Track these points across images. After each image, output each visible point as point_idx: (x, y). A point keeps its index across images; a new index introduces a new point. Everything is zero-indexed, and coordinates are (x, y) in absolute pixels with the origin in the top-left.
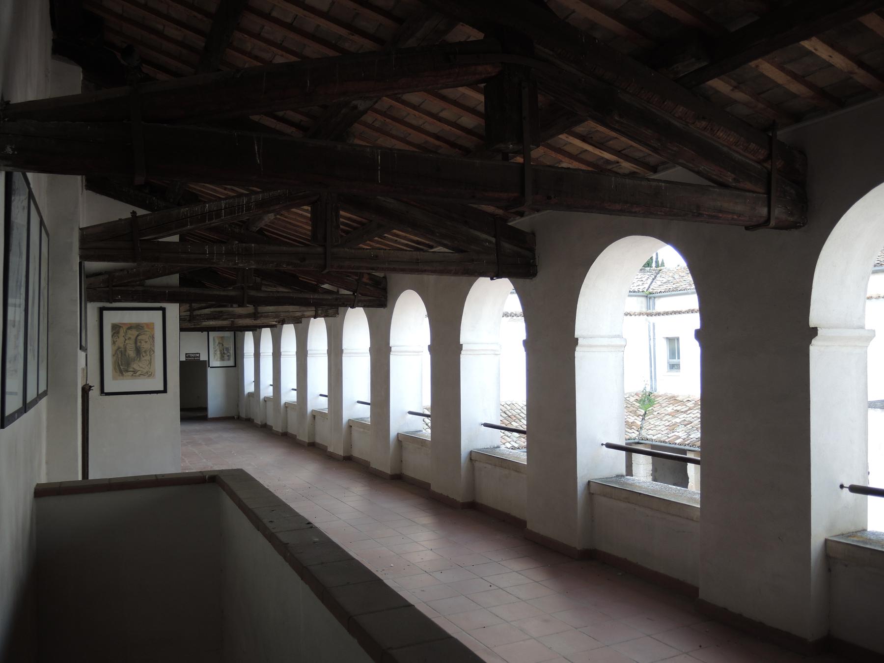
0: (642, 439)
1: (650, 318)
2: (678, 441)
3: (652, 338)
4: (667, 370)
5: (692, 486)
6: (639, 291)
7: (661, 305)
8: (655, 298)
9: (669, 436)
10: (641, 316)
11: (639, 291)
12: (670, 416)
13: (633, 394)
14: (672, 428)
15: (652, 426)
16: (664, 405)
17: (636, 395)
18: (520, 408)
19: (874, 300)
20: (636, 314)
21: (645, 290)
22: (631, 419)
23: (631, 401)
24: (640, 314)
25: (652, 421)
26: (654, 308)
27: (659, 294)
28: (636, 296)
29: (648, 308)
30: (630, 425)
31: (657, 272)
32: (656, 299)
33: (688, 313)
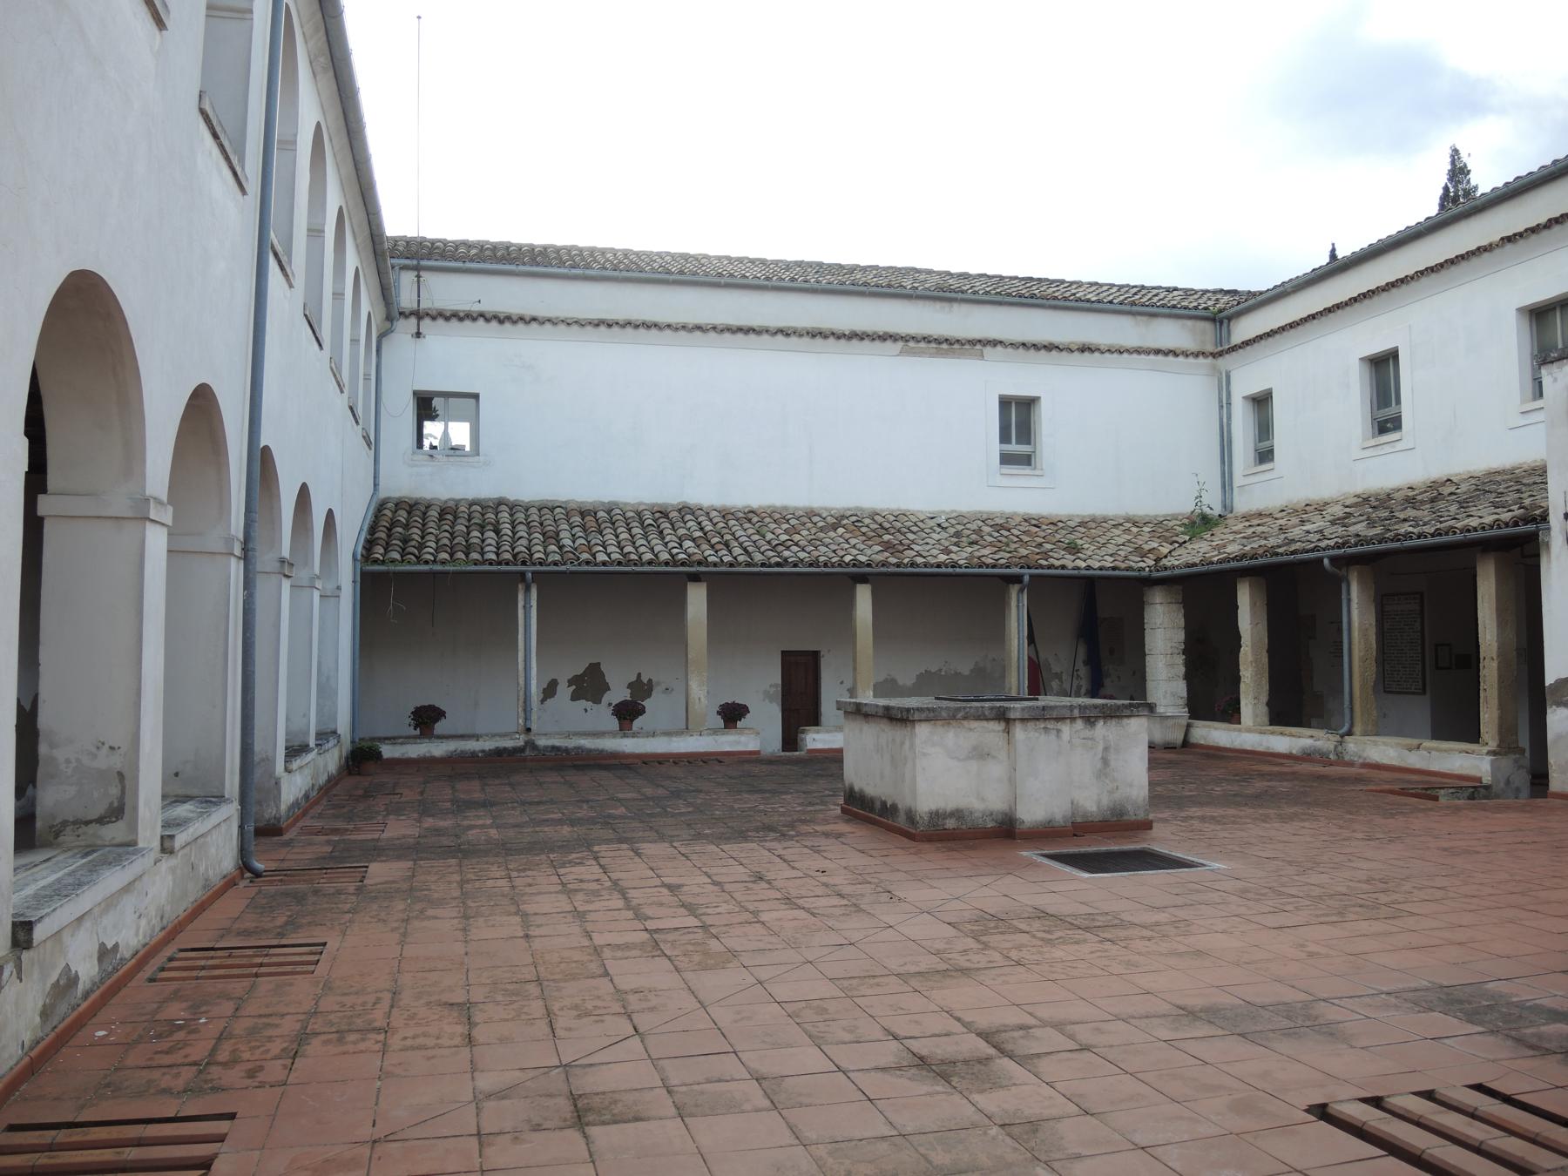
7: (1245, 328)
24: (1196, 355)
26: (1229, 342)
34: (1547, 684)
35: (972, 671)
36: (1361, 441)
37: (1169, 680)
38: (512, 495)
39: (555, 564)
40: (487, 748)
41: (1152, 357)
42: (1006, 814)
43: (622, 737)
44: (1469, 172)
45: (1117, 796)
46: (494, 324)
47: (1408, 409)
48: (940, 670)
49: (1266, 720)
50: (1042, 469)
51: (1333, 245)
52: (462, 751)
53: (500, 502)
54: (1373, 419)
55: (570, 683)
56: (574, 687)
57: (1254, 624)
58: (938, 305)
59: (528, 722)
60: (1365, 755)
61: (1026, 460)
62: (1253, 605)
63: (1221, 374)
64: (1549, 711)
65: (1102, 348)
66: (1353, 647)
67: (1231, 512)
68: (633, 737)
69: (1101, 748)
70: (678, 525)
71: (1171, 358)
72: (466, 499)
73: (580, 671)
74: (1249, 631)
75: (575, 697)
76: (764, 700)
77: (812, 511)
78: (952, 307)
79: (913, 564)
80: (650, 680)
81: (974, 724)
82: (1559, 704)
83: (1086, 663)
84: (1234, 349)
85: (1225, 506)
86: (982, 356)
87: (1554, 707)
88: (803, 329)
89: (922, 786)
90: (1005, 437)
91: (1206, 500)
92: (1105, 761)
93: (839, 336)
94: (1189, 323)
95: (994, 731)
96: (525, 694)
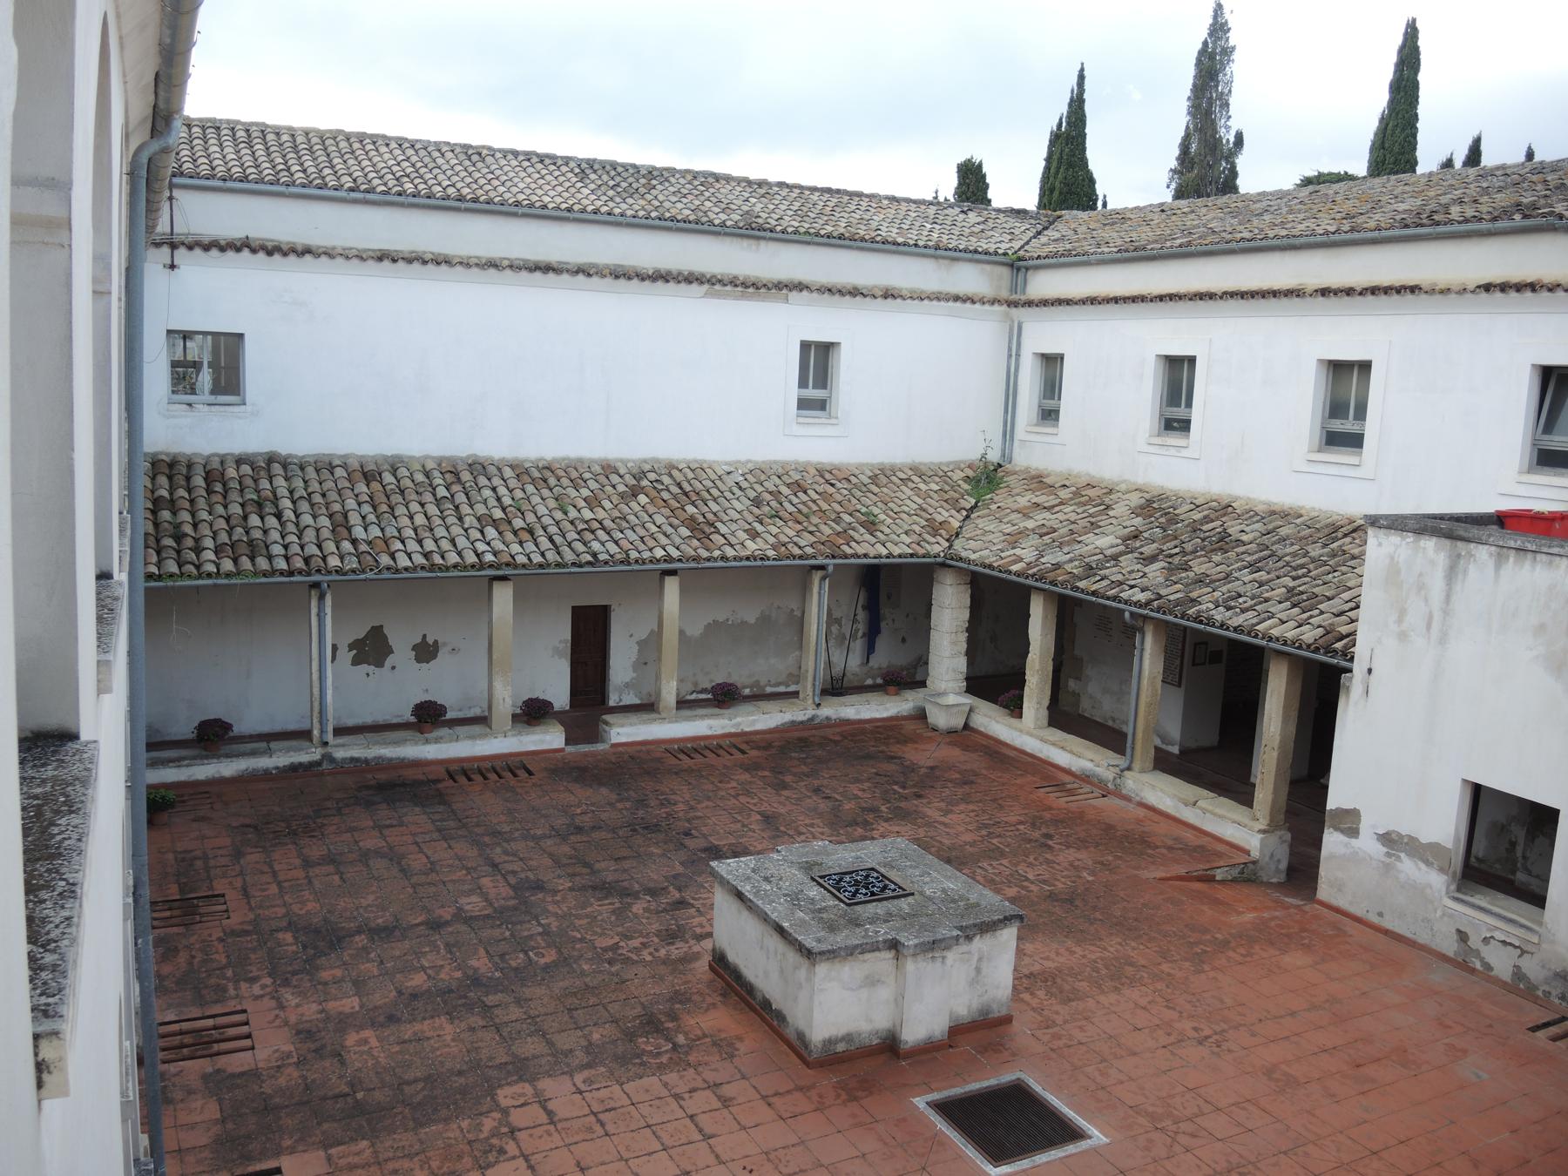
0: (952, 559)
1: (1014, 311)
2: (1014, 568)
3: (1014, 354)
4: (1035, 421)
5: (1033, 660)
6: (996, 253)
7: (1044, 284)
8: (1027, 269)
9: (1003, 555)
10: (889, 300)
11: (996, 253)
12: (1020, 515)
13: (962, 466)
14: (1014, 540)
15: (979, 532)
16: (1015, 491)
17: (969, 467)
18: (713, 477)
19: (1453, 296)
20: (985, 300)
21: (1010, 252)
22: (942, 515)
23: (955, 478)
24: (993, 302)
25: (982, 522)
26: (1024, 292)
27: (1036, 262)
28: (970, 260)
29: (1011, 291)
30: (934, 528)
31: (1051, 219)
32: (1030, 273)
33: (1084, 303)
34: (1328, 808)
35: (757, 619)
36: (1147, 435)
37: (953, 656)
38: (283, 450)
39: (353, 571)
40: (281, 765)
41: (951, 304)
42: (890, 1031)
43: (424, 744)
44: (1229, 29)
45: (985, 998)
46: (261, 255)
47: (1198, 414)
48: (728, 620)
49: (1045, 722)
50: (837, 418)
51: (1082, 64)
52: (254, 770)
53: (271, 459)
54: (1161, 415)
55: (351, 647)
56: (355, 652)
57: (1044, 635)
58: (745, 243)
59: (324, 736)
60: (1143, 794)
61: (821, 405)
62: (1045, 618)
63: (1013, 322)
64: (1326, 831)
65: (904, 293)
66: (1141, 692)
67: (1010, 463)
68: (436, 743)
69: (976, 957)
70: (473, 493)
71: (968, 305)
72: (232, 455)
73: (361, 635)
74: (1039, 643)
75: (356, 662)
76: (553, 656)
77: (609, 466)
78: (759, 244)
79: (724, 558)
80: (436, 642)
81: (868, 956)
82: (1336, 829)
83: (864, 608)
84: (1029, 303)
85: (1003, 455)
86: (786, 300)
87: (1331, 830)
88: (607, 266)
89: (818, 1016)
90: (803, 383)
91: (989, 451)
92: (978, 970)
93: (642, 277)
94: (988, 267)
95: (884, 959)
96: (321, 704)
